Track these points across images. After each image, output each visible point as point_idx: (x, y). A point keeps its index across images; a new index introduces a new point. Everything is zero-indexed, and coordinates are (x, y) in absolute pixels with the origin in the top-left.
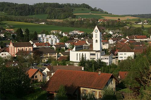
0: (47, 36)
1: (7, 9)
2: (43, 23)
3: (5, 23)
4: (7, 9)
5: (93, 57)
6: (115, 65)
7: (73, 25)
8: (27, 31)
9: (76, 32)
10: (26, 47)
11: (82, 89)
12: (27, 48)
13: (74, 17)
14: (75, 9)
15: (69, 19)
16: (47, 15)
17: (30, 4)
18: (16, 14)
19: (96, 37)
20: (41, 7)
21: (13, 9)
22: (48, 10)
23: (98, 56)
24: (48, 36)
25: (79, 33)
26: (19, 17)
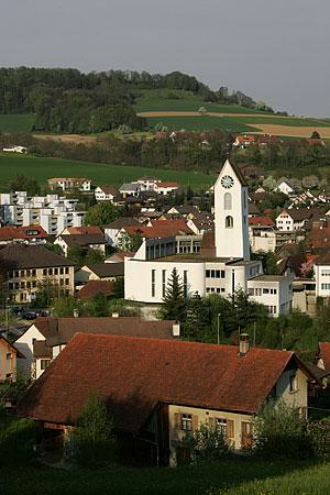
0: (35, 199)
2: (19, 149)
5: (214, 282)
9: (148, 184)
11: (173, 409)
13: (141, 125)
14: (141, 95)
16: (31, 119)
19: (228, 205)
22: (36, 95)
23: (234, 282)
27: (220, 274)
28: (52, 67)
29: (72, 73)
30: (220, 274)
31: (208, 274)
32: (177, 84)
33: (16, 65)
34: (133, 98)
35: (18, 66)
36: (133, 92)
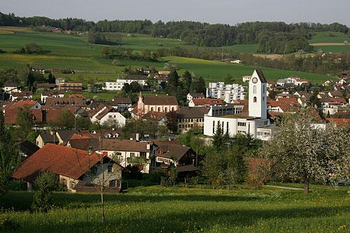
0: (227, 86)
1: (186, 35)
2: (238, 61)
3: (166, 60)
4: (186, 35)
5: (241, 128)
6: (210, 147)
7: (300, 66)
8: (188, 75)
9: (293, 80)
10: (158, 105)
11: (61, 176)
12: (161, 106)
13: (311, 49)
14: (315, 35)
15: (297, 55)
16: (257, 46)
17: (231, 25)
18: (201, 43)
19: (254, 92)
20: (249, 29)
21: (197, 33)
22: (261, 35)
23: (251, 129)
24: (229, 87)
25: (296, 83)
26: (202, 49)
27: (244, 124)
28: (32, 16)
29: (281, 24)
30: (244, 124)
31: (239, 124)
32: (335, 29)
33: (254, 20)
34: (310, 36)
35: (255, 21)
36: (310, 33)
